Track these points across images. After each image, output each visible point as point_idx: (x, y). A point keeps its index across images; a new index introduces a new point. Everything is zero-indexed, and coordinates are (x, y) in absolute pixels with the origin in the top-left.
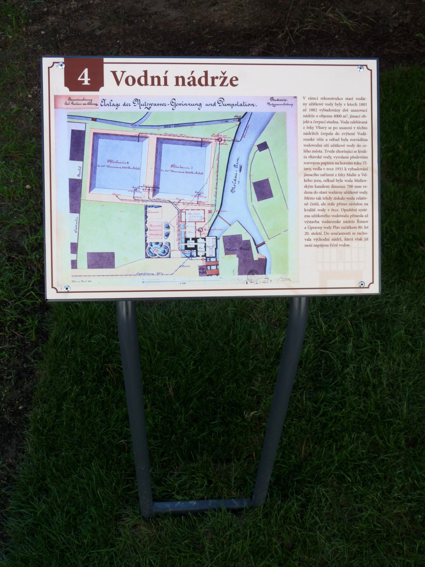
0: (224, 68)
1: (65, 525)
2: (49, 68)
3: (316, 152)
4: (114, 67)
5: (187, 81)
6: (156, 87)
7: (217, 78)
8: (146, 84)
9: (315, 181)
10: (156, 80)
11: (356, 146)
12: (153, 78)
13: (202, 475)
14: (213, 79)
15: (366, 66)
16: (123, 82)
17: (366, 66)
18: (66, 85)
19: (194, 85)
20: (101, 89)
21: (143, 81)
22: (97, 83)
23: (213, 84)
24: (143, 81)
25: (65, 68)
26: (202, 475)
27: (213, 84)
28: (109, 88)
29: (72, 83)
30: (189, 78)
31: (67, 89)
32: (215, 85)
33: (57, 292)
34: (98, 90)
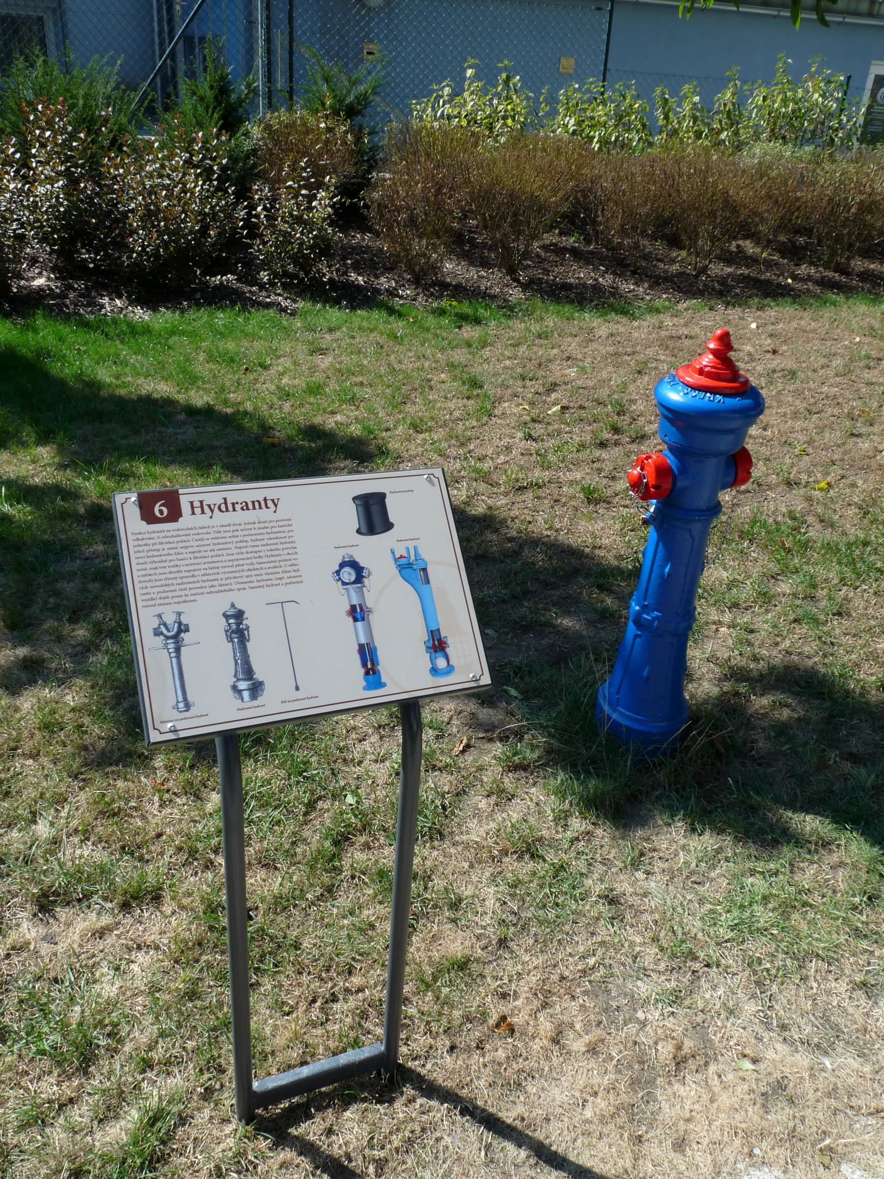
0: (224, 495)
6: (258, 511)
8: (227, 510)
10: (257, 504)
14: (233, 504)
18: (143, 518)
20: (180, 519)
21: (223, 508)
22: (175, 514)
23: (234, 510)
24: (223, 508)
27: (234, 510)
28: (186, 519)
29: (148, 517)
31: (144, 523)
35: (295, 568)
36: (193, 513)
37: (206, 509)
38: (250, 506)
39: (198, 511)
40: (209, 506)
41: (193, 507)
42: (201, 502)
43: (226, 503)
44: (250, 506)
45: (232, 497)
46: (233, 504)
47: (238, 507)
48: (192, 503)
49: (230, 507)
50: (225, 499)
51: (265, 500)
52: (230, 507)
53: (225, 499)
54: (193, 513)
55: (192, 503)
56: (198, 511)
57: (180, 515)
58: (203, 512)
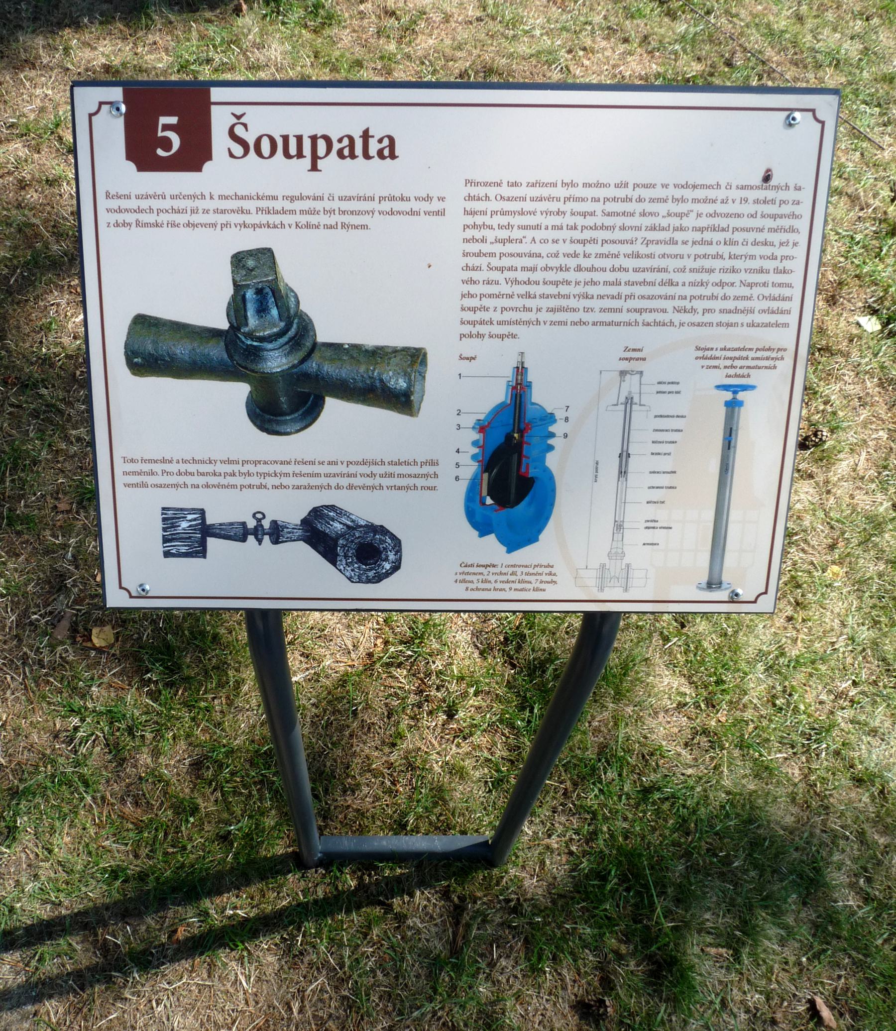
5: (336, 146)
8: (314, 139)
10: (293, 150)
12: (300, 155)
15: (131, 597)
17: (131, 597)
18: (129, 157)
19: (353, 156)
20: (207, 166)
21: (322, 146)
22: (194, 155)
24: (322, 146)
25: (127, 115)
28: (223, 171)
29: (143, 152)
30: (340, 141)
38: (359, 150)
43: (315, 158)
44: (359, 150)
50: (314, 168)
51: (366, 136)
53: (314, 168)
57: (207, 155)
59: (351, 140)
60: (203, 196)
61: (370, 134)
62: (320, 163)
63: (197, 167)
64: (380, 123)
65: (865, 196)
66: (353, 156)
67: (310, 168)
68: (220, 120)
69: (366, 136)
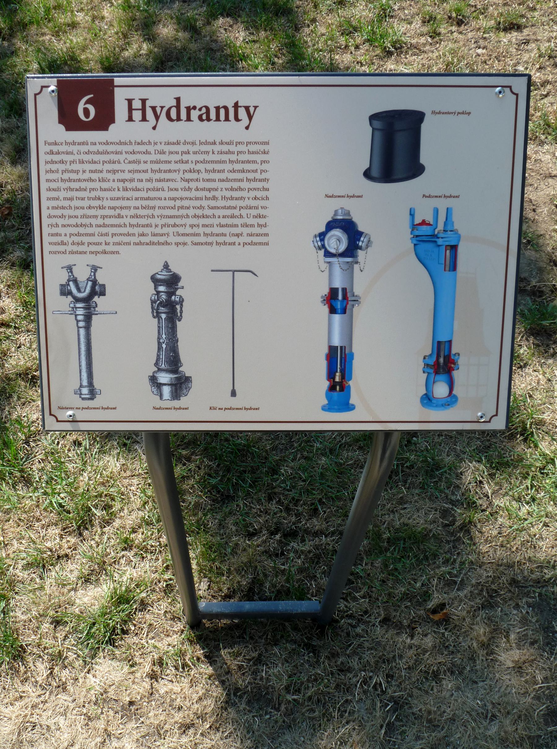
0: (177, 92)
1: (137, 720)
2: (36, 95)
3: (57, 208)
4: (137, 94)
6: (222, 124)
7: (194, 108)
8: (179, 119)
9: (89, 244)
10: (222, 111)
11: (193, 190)
13: (314, 492)
14: (188, 109)
15: (510, 87)
16: (163, 116)
17: (510, 87)
18: (60, 122)
19: (208, 119)
20: (112, 127)
21: (173, 114)
22: (104, 120)
23: (189, 119)
24: (173, 114)
26: (314, 492)
27: (189, 119)
28: (120, 128)
29: (69, 119)
31: (62, 127)
32: (147, 119)
33: (496, 415)
34: (106, 128)
35: (262, 221)
36: (130, 119)
37: (149, 112)
38: (213, 115)
39: (137, 115)
40: (154, 108)
41: (130, 109)
42: (144, 101)
43: (178, 107)
44: (213, 115)
45: (189, 98)
46: (188, 109)
47: (195, 114)
48: (130, 101)
49: (183, 115)
50: (178, 100)
52: (183, 115)
53: (178, 100)
54: (130, 119)
55: (130, 101)
56: (137, 115)
58: (144, 119)
59: (207, 109)
60: (131, 143)
61: (239, 105)
62: (174, 103)
63: (105, 128)
64: (246, 97)
65: (531, 427)
66: (208, 119)
67: (127, 119)
68: (120, 98)
69: (236, 106)
